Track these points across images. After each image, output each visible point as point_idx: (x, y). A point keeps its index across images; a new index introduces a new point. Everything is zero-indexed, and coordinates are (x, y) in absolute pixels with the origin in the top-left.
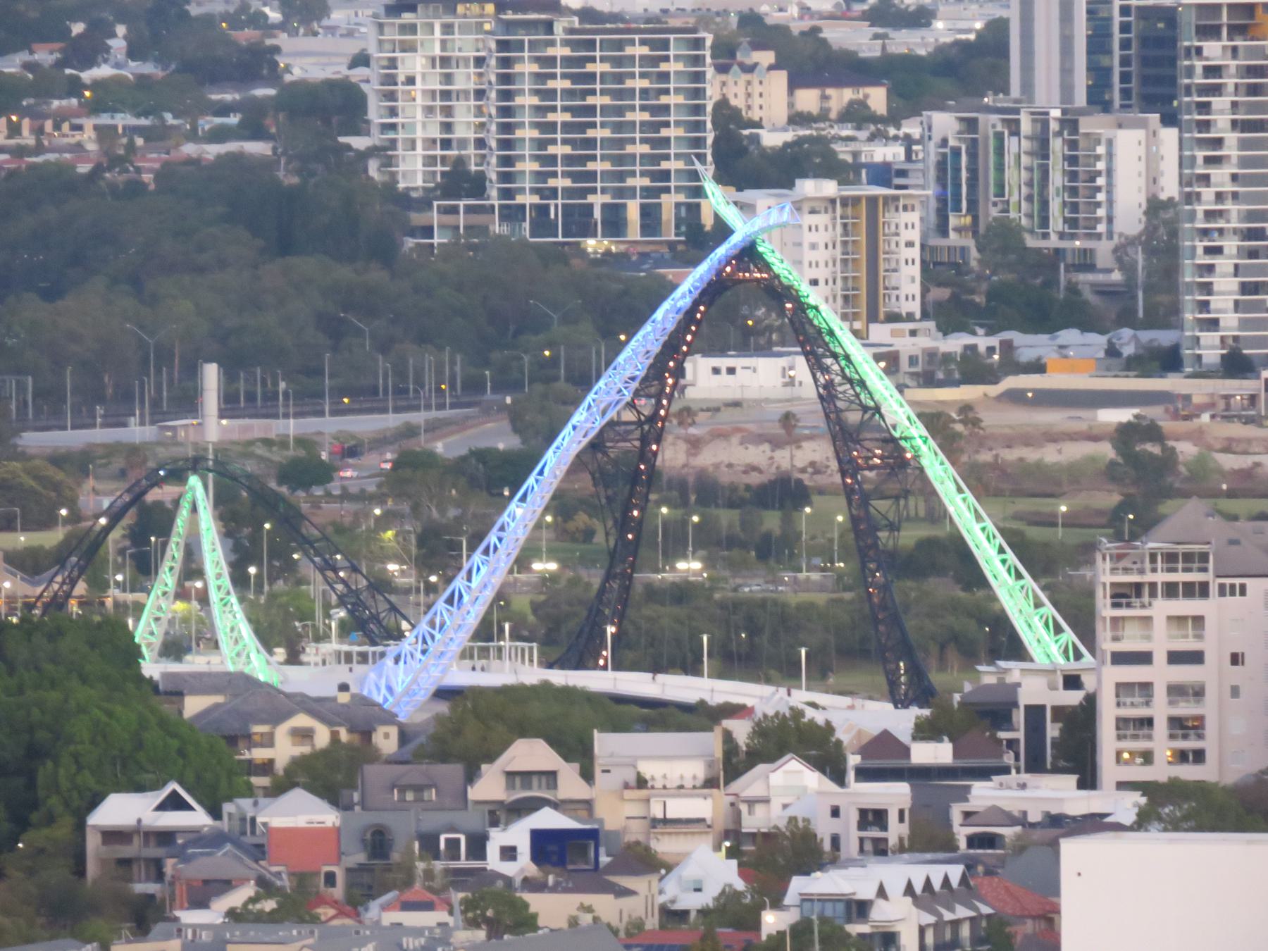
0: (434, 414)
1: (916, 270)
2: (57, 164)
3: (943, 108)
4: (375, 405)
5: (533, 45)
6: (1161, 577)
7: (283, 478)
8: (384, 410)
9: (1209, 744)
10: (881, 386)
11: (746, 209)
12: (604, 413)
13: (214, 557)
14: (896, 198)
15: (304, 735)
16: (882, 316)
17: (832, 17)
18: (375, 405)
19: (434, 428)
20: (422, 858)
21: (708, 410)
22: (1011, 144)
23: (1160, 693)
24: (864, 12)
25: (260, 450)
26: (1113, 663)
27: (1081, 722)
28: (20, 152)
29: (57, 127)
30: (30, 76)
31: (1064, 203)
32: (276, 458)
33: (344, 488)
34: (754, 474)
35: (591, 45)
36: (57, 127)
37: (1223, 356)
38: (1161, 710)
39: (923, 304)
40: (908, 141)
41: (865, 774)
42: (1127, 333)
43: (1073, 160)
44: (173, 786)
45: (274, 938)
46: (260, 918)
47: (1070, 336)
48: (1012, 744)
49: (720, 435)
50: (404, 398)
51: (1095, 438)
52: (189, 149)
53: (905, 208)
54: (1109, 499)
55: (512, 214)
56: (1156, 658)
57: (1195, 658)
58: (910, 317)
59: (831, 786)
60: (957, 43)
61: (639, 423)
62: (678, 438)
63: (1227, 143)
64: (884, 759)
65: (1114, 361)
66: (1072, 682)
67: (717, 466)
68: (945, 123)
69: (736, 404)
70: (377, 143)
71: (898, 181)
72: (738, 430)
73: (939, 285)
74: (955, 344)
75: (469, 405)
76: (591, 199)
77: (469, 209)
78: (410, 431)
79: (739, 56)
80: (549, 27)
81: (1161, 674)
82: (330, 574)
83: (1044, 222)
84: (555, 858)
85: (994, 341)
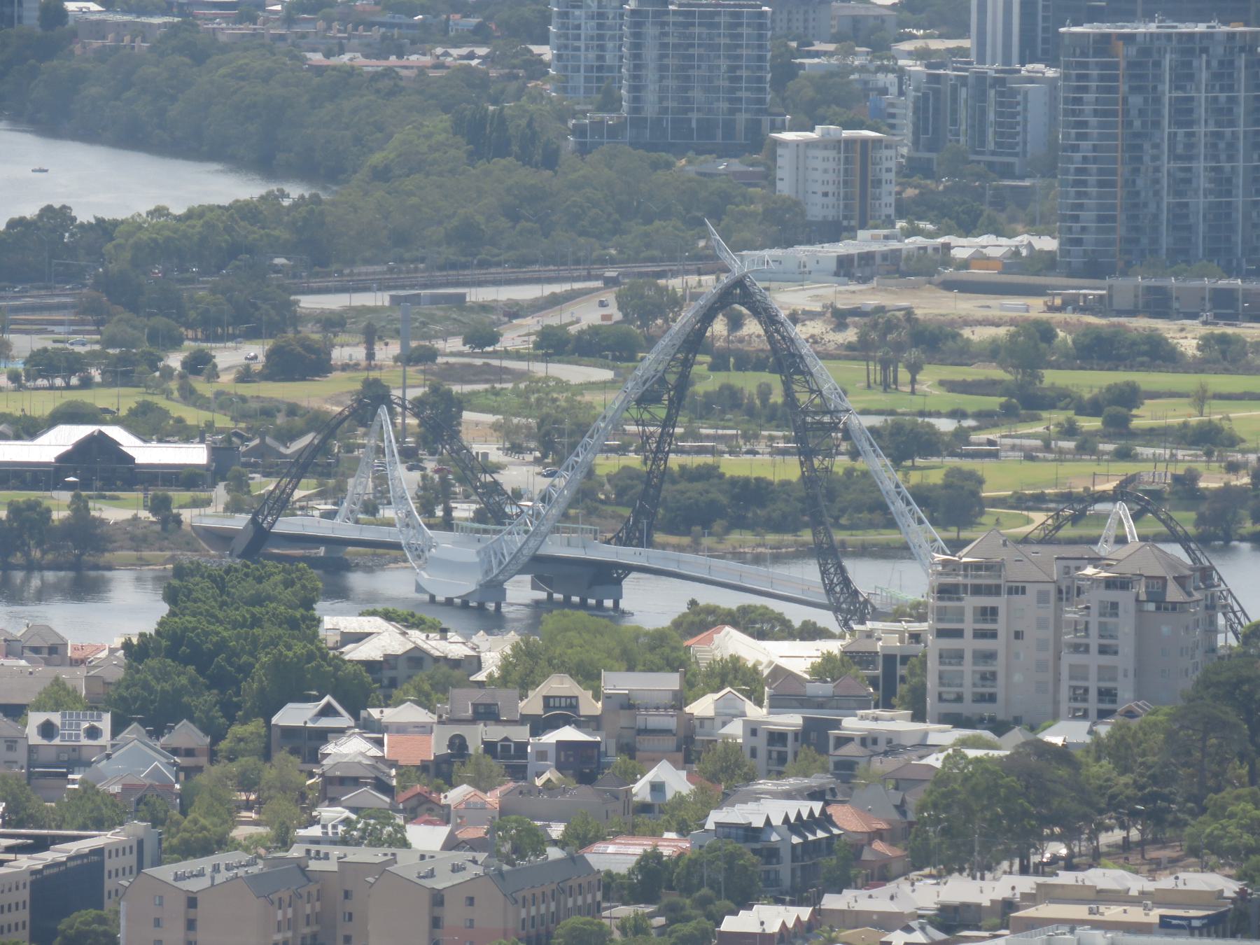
12: (644, 383)
31: (996, 132)
35: (692, 14)
37: (1085, 263)
43: (1001, 104)
53: (887, 147)
76: (690, 115)
81: (968, 644)
83: (983, 143)
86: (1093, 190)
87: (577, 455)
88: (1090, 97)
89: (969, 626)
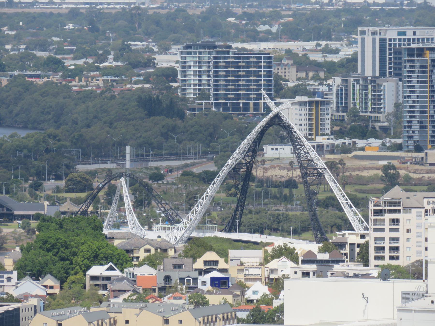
0: (192, 161)
1: (329, 122)
2: (91, 90)
3: (338, 76)
4: (177, 158)
5: (224, 58)
6: (387, 208)
7: (150, 178)
8: (179, 160)
9: (400, 254)
10: (314, 155)
11: (277, 104)
13: (128, 201)
14: (324, 102)
15: (148, 251)
16: (319, 134)
17: (311, 51)
18: (177, 158)
19: (193, 165)
20: (180, 285)
21: (270, 160)
22: (357, 87)
23: (387, 240)
24: (320, 49)
25: (144, 171)
26: (374, 231)
27: (365, 247)
28: (82, 87)
29: (92, 80)
30: (86, 66)
31: (372, 103)
32: (149, 173)
33: (167, 181)
34: (283, 178)
35: (240, 58)
36: (92, 80)
38: (387, 245)
39: (331, 131)
40: (329, 85)
41: (304, 262)
42: (388, 139)
43: (374, 91)
44: (110, 264)
45: (136, 307)
46: (132, 301)
47: (372, 140)
48: (346, 254)
49: (273, 167)
50: (185, 155)
51: (378, 169)
52: (129, 86)
54: (382, 186)
55: (217, 105)
56: (386, 230)
57: (397, 230)
58: (328, 135)
59: (294, 265)
60: (346, 58)
61: (246, 164)
62: (261, 168)
63: (416, 87)
64: (309, 259)
65: (385, 147)
66: (363, 237)
67: (272, 176)
68: (338, 80)
69: (278, 159)
70: (180, 85)
71: (325, 97)
72: (278, 166)
73: (336, 126)
74: (340, 141)
75: (204, 158)
77: (206, 103)
78: (187, 166)
79: (283, 62)
80: (228, 53)
81: (387, 235)
82: (160, 205)
83: (366, 108)
84: (217, 285)
85: (351, 141)
86: (417, 114)
87: (208, 193)
88: (414, 75)
89: (387, 226)
